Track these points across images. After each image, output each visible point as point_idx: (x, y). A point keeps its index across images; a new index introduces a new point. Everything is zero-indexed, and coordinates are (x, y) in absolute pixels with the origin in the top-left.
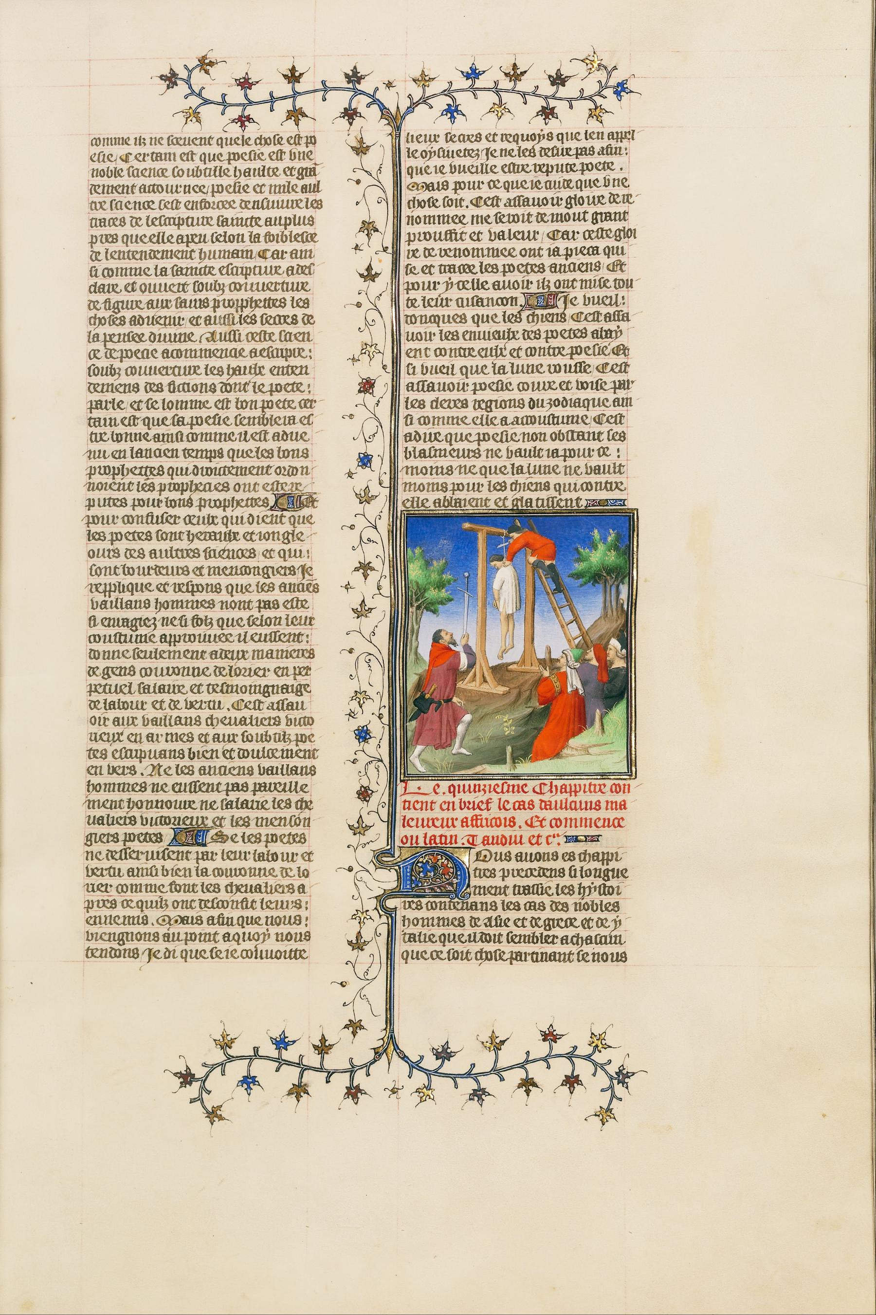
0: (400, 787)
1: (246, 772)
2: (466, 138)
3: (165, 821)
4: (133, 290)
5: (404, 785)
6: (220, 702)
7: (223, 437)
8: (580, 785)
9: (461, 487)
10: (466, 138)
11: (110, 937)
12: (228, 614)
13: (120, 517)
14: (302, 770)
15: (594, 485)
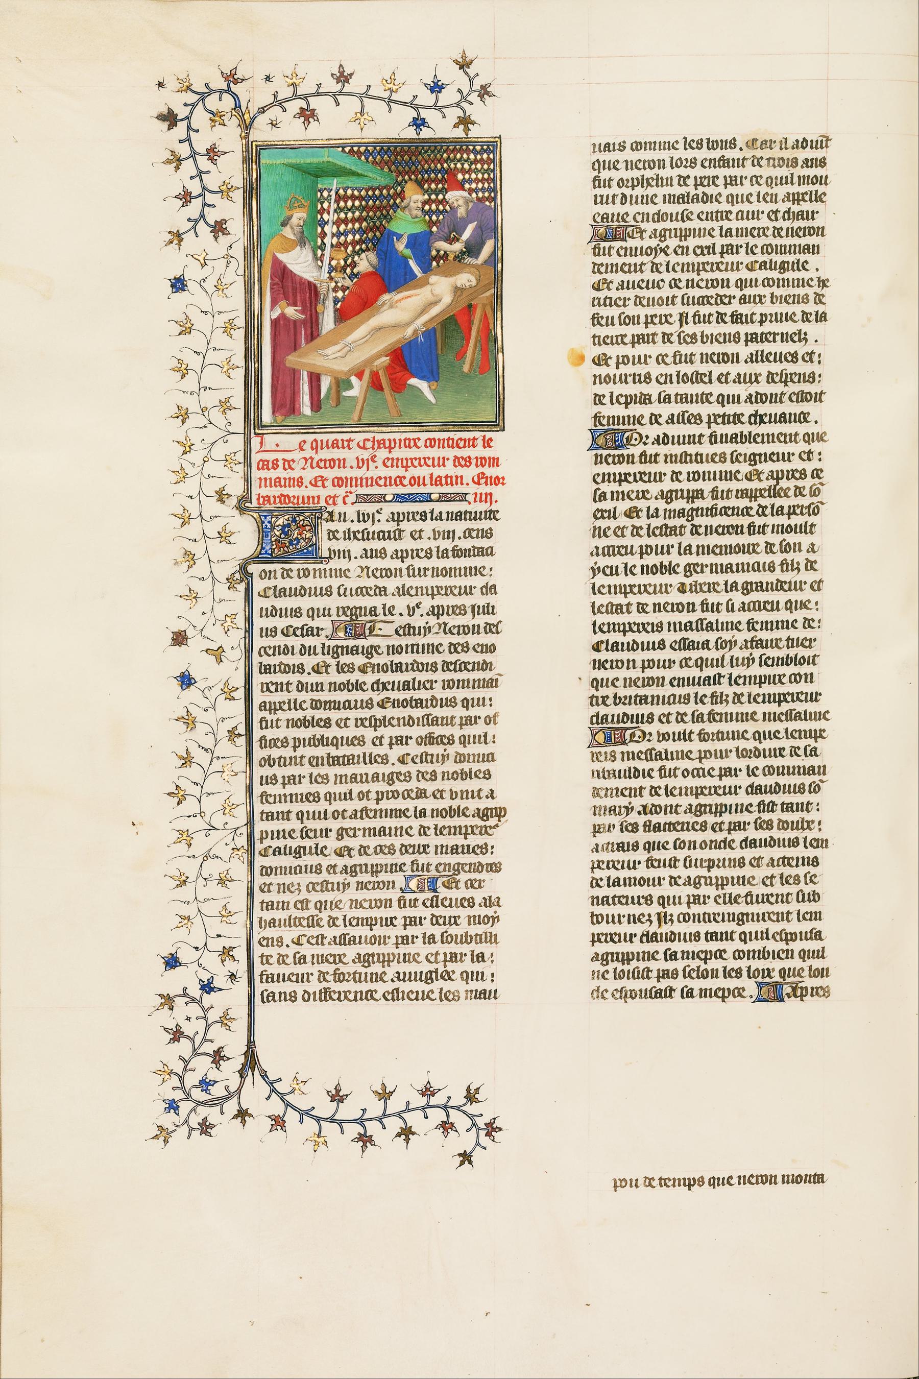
0: (255, 441)
1: (275, 943)
2: (643, 588)
5: (259, 439)
6: (260, 487)
9: (381, 886)
10: (643, 588)
12: (653, 837)
14: (278, 815)
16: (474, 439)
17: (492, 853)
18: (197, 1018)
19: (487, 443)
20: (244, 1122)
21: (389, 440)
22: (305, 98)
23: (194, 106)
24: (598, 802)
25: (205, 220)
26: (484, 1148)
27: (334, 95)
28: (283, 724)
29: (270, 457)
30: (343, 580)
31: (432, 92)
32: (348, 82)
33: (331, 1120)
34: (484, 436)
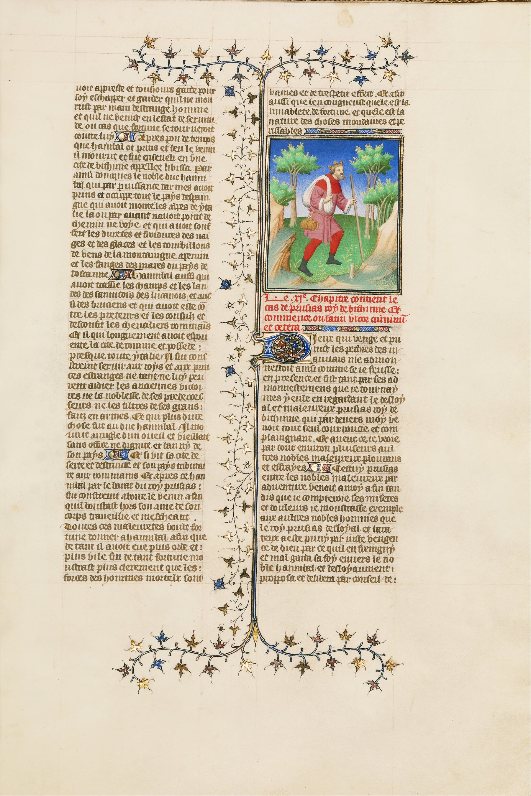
0: (263, 298)
8: (333, 297)
13: (352, 578)
15: (101, 475)
20: (303, 671)
21: (330, 297)
22: (233, 61)
26: (146, 70)
27: (186, 67)
28: (280, 428)
29: (274, 304)
30: (142, 501)
31: (128, 674)
32: (180, 75)
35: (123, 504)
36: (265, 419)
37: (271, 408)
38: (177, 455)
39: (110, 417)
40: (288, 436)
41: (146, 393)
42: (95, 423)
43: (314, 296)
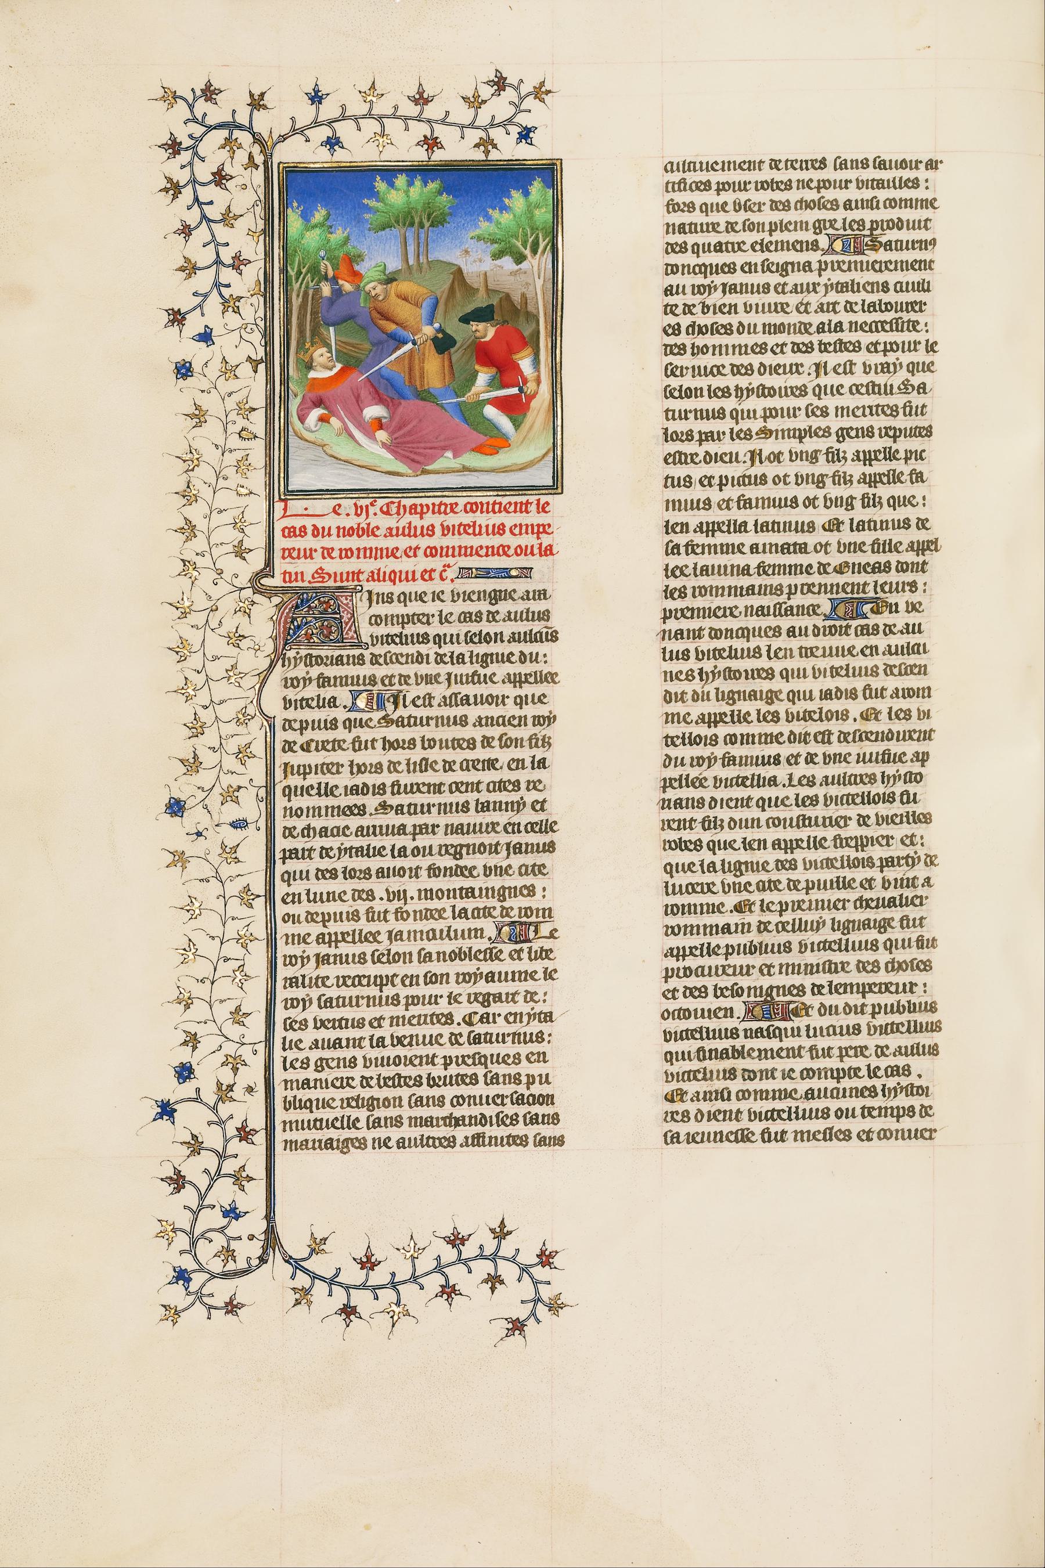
0: (279, 507)
3: (737, 992)
4: (431, 579)
5: (282, 504)
7: (806, 1135)
11: (339, 1063)
16: (528, 503)
17: (549, 1042)
18: (240, 1238)
19: (543, 508)
21: (421, 505)
23: (191, 164)
24: (674, 561)
25: (188, 103)
29: (298, 523)
33: (363, 1286)
34: (538, 500)
35: (355, 763)
36: (793, 718)
37: (829, 367)
38: (895, 285)
39: (434, 810)
40: (503, 888)
41: (327, 846)
42: (867, 687)
43: (388, 505)
